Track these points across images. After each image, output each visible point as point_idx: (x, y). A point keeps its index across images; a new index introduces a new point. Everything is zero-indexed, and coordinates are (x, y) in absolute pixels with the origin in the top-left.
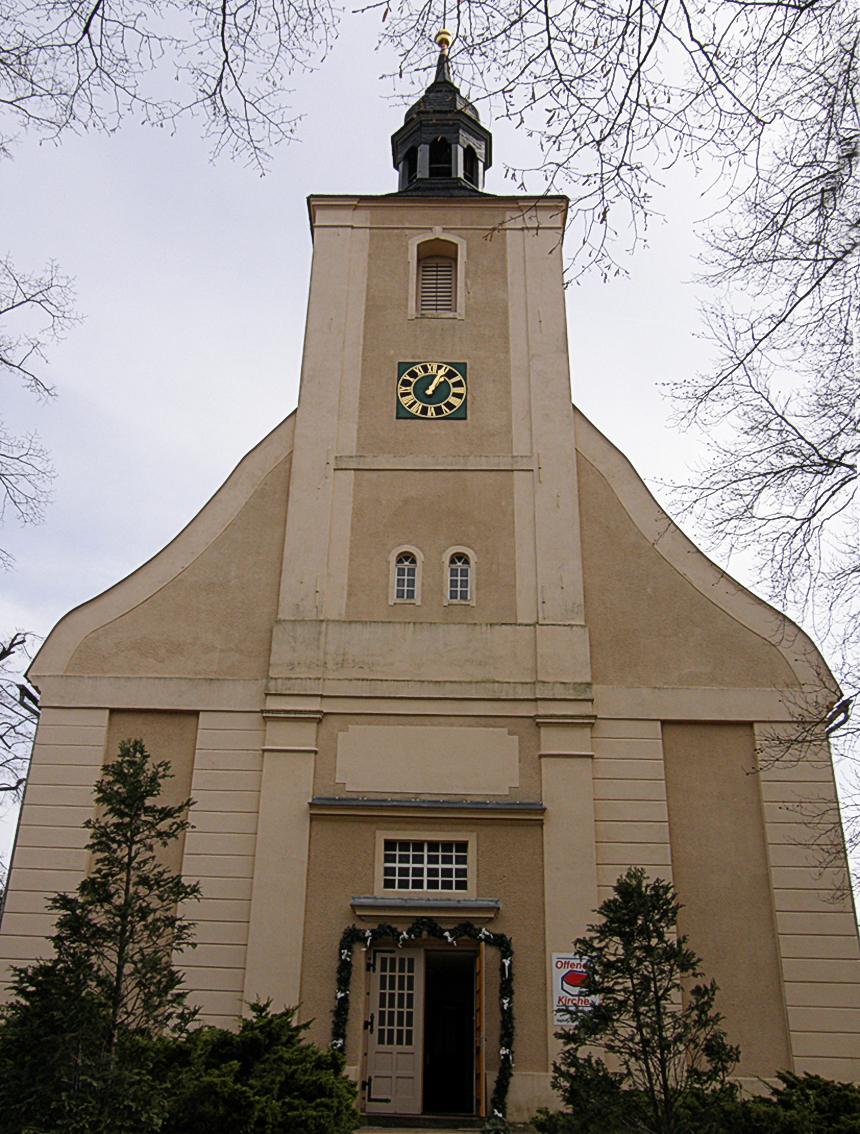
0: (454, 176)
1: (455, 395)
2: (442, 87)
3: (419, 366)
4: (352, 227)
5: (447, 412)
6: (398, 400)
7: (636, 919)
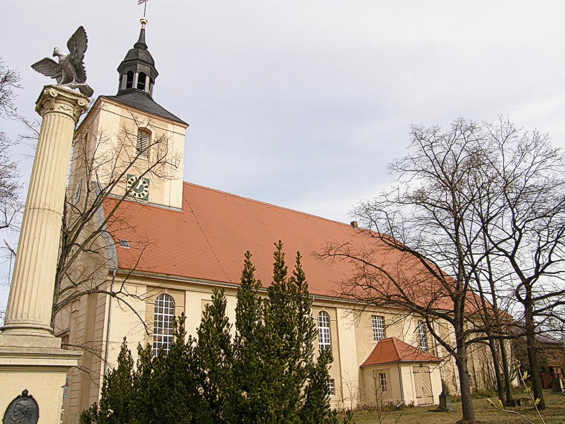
0: (133, 88)
1: (145, 191)
2: (141, 45)
3: (134, 177)
4: (114, 113)
5: (142, 197)
6: (149, 185)
7: (197, 392)
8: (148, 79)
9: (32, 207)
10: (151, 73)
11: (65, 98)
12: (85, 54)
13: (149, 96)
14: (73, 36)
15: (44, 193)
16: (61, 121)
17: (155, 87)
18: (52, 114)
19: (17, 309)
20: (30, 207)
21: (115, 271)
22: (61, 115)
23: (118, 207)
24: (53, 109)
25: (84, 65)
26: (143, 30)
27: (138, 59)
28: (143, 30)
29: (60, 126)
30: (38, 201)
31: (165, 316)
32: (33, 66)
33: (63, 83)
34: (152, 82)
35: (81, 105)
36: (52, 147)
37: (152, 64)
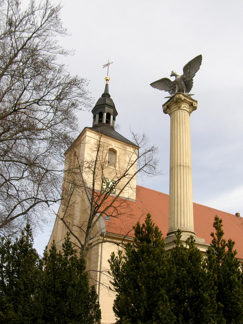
0: (103, 123)
2: (106, 95)
8: (112, 117)
9: (179, 164)
10: (114, 114)
11: (186, 101)
12: (196, 74)
13: (113, 128)
14: (190, 63)
17: (116, 123)
18: (180, 111)
20: (177, 164)
21: (105, 234)
23: (122, 192)
24: (180, 108)
26: (107, 85)
27: (106, 104)
28: (107, 85)
29: (186, 118)
30: (182, 162)
32: (151, 84)
34: (114, 119)
36: (184, 130)
37: (113, 107)
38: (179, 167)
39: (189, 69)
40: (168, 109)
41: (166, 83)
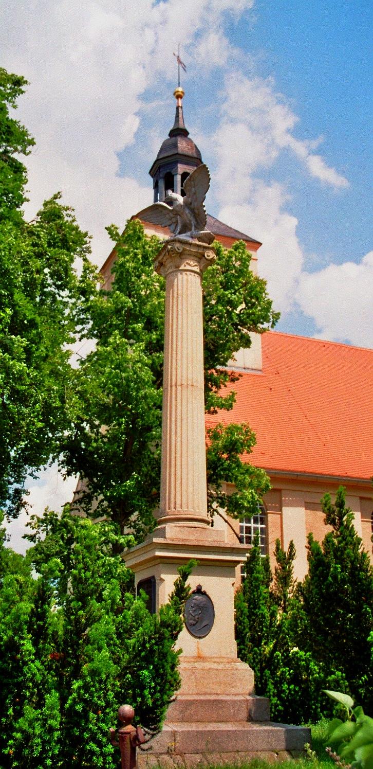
15: (184, 367)
16: (189, 280)
19: (175, 499)
20: (171, 383)
22: (188, 273)
25: (204, 209)
27: (177, 154)
30: (179, 377)
31: (247, 537)
33: (180, 233)
35: (208, 258)
38: (174, 388)
39: (194, 187)
40: (162, 267)
41: (162, 212)
